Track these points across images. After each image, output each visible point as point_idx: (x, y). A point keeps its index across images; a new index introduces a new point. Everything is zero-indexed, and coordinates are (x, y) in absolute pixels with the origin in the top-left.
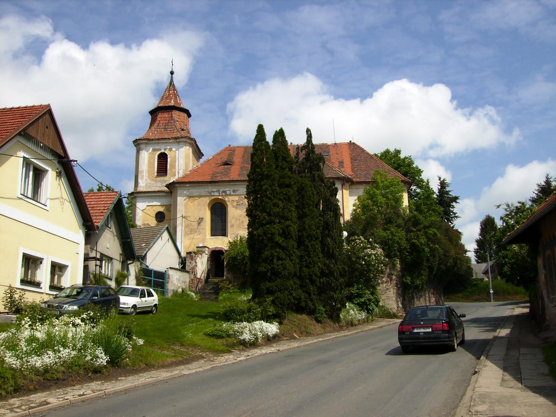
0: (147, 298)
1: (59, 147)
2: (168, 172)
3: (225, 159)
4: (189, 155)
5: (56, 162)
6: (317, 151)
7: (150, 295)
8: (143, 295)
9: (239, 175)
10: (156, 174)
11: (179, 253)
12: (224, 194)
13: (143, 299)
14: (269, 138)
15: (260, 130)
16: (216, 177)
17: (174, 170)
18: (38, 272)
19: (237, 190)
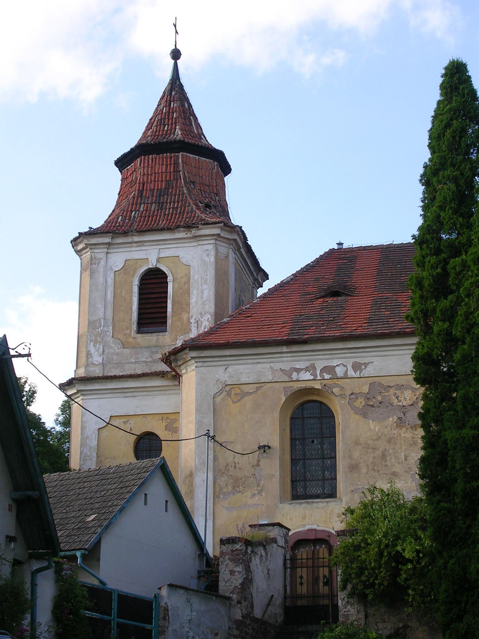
2: (169, 321)
4: (226, 273)
9: (370, 321)
10: (134, 327)
12: (327, 376)
16: (304, 328)
17: (185, 316)
19: (366, 365)
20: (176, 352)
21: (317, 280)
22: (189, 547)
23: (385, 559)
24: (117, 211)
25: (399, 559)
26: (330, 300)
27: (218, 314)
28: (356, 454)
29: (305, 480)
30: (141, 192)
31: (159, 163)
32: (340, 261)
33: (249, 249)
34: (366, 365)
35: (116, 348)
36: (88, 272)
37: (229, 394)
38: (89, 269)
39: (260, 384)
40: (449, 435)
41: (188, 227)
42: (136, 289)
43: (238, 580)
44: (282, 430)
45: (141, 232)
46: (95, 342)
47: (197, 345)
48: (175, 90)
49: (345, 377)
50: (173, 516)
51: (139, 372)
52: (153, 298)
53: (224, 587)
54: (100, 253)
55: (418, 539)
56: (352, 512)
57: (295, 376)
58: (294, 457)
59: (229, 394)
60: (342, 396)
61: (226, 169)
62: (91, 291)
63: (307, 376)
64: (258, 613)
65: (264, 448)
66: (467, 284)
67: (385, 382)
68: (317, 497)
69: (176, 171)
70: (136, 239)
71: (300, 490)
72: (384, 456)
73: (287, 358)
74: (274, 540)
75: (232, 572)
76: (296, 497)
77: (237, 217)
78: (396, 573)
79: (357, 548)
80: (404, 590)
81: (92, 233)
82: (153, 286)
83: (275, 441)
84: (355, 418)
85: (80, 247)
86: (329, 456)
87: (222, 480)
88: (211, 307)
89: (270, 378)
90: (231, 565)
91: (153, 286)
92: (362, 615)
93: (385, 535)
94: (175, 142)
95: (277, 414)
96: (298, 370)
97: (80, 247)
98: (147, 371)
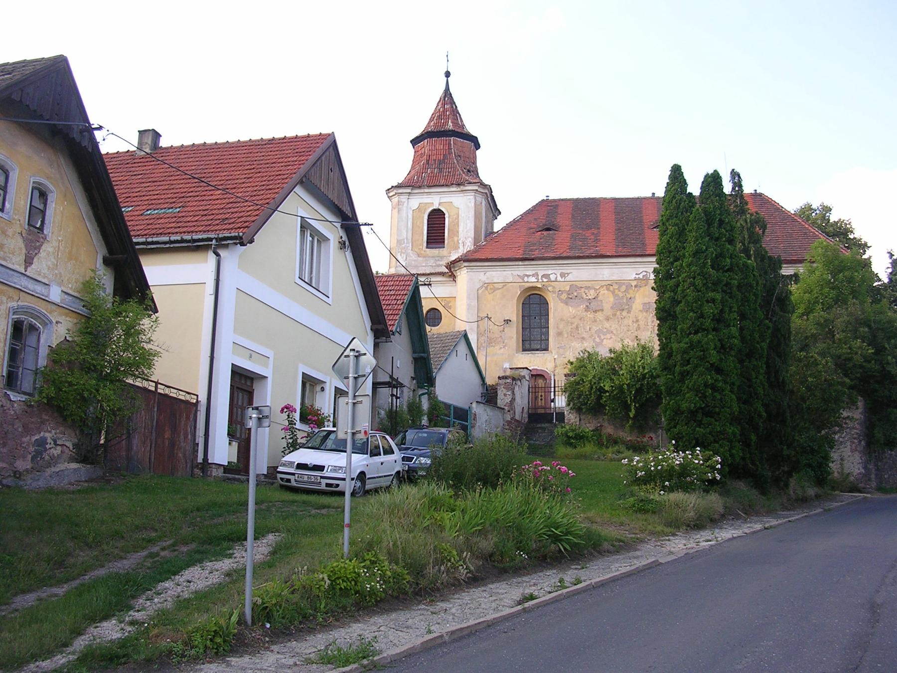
0: (383, 458)
1: (346, 200)
2: (446, 242)
3: (542, 221)
4: (480, 213)
5: (338, 225)
6: (752, 207)
7: (389, 451)
8: (375, 453)
9: (571, 248)
10: (425, 244)
11: (483, 379)
12: (545, 280)
13: (378, 459)
14: (694, 188)
15: (676, 174)
16: (531, 250)
17: (456, 239)
18: (319, 396)
19: (568, 274)
20: (454, 262)
21: (535, 219)
22: (476, 379)
23: (594, 390)
24: (413, 172)
25: (602, 390)
26: (545, 233)
27: (476, 240)
28: (561, 326)
29: (530, 340)
30: (428, 161)
31: (439, 144)
32: (548, 207)
33: (492, 197)
34: (568, 274)
35: (414, 257)
36: (396, 210)
37: (486, 288)
38: (397, 207)
39: (505, 283)
40: (675, 346)
41: (459, 185)
42: (426, 222)
43: (508, 399)
44: (518, 310)
45: (429, 187)
46: (401, 253)
47: (468, 259)
48: (447, 96)
49: (556, 281)
50: (470, 363)
51: (428, 272)
52: (436, 228)
53: (500, 403)
54: (404, 198)
55: (611, 379)
56: (572, 363)
57: (526, 279)
58: (526, 326)
59: (486, 288)
60: (554, 292)
61: (478, 146)
62: (398, 221)
63: (533, 279)
64: (517, 417)
65: (507, 321)
66: (684, 275)
67: (579, 284)
68: (537, 350)
69: (450, 149)
70: (426, 191)
71: (527, 346)
72: (577, 327)
73: (521, 268)
74: (524, 377)
75: (505, 395)
76: (524, 350)
77: (485, 175)
78: (599, 398)
79: (578, 383)
80: (604, 406)
81: (399, 186)
82: (436, 219)
83: (514, 318)
84: (562, 305)
85: (391, 194)
86: (545, 327)
87: (482, 339)
88: (472, 234)
89: (511, 280)
90: (505, 391)
91: (436, 219)
92: (578, 419)
93: (594, 377)
94: (449, 131)
95: (515, 301)
96: (528, 276)
97: (391, 194)
98: (433, 271)
